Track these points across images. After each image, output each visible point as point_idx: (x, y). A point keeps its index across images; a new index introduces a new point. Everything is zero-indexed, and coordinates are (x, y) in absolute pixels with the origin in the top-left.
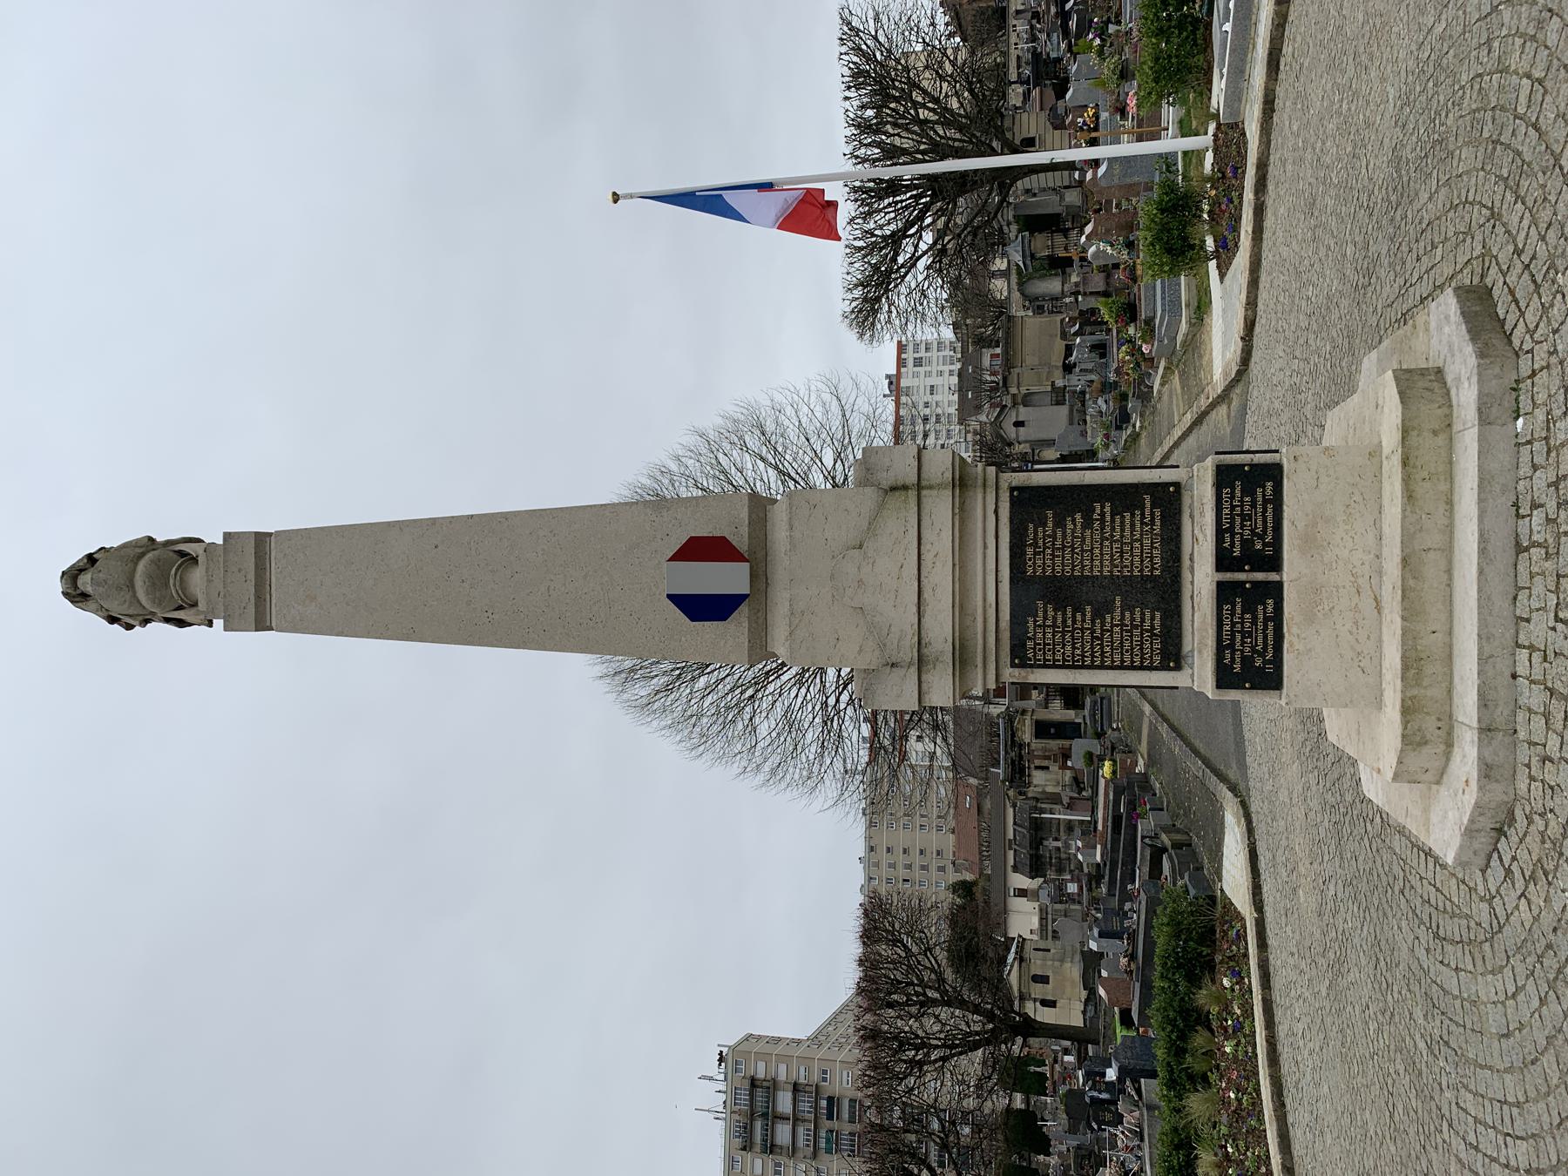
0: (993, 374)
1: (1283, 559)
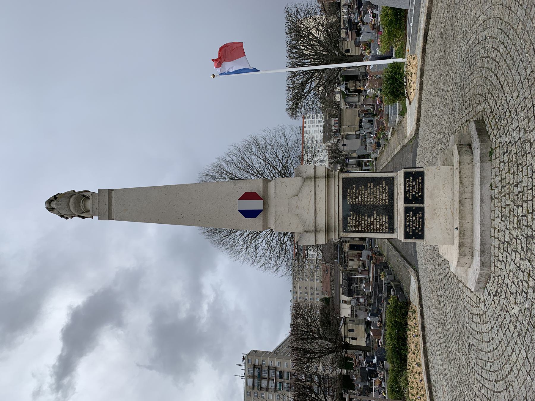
0: (335, 127)
1: (424, 200)
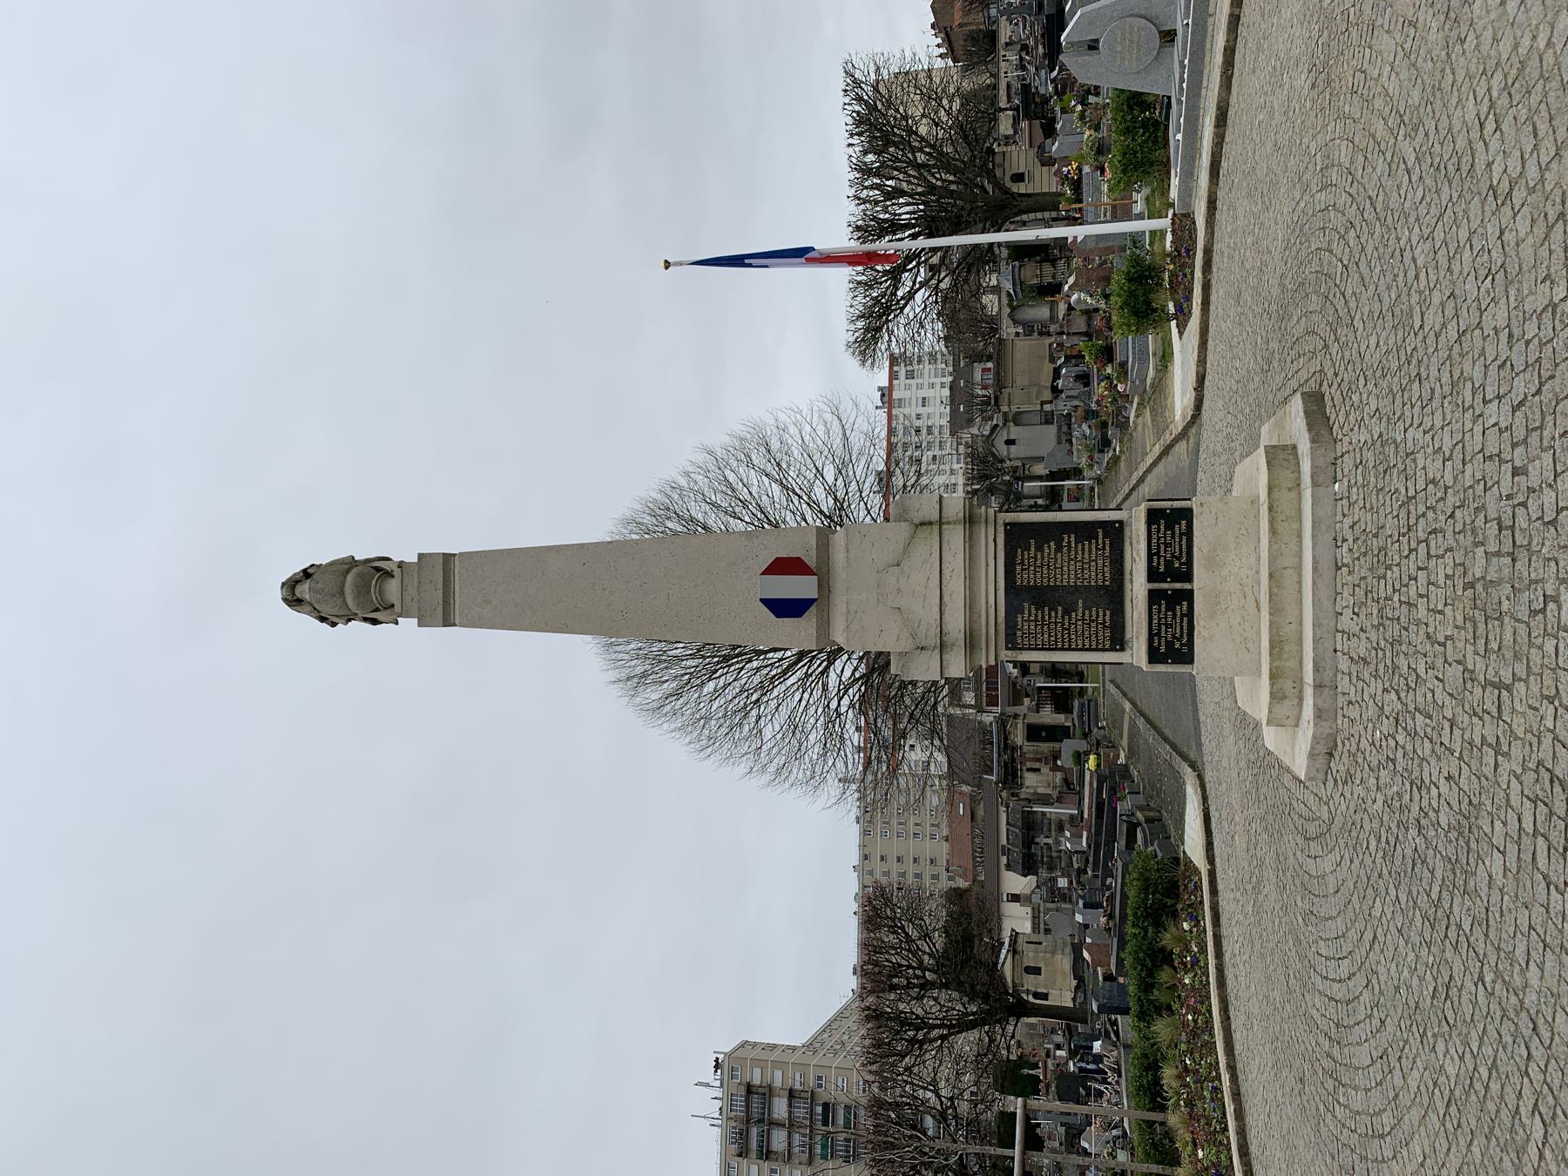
0: (985, 387)
